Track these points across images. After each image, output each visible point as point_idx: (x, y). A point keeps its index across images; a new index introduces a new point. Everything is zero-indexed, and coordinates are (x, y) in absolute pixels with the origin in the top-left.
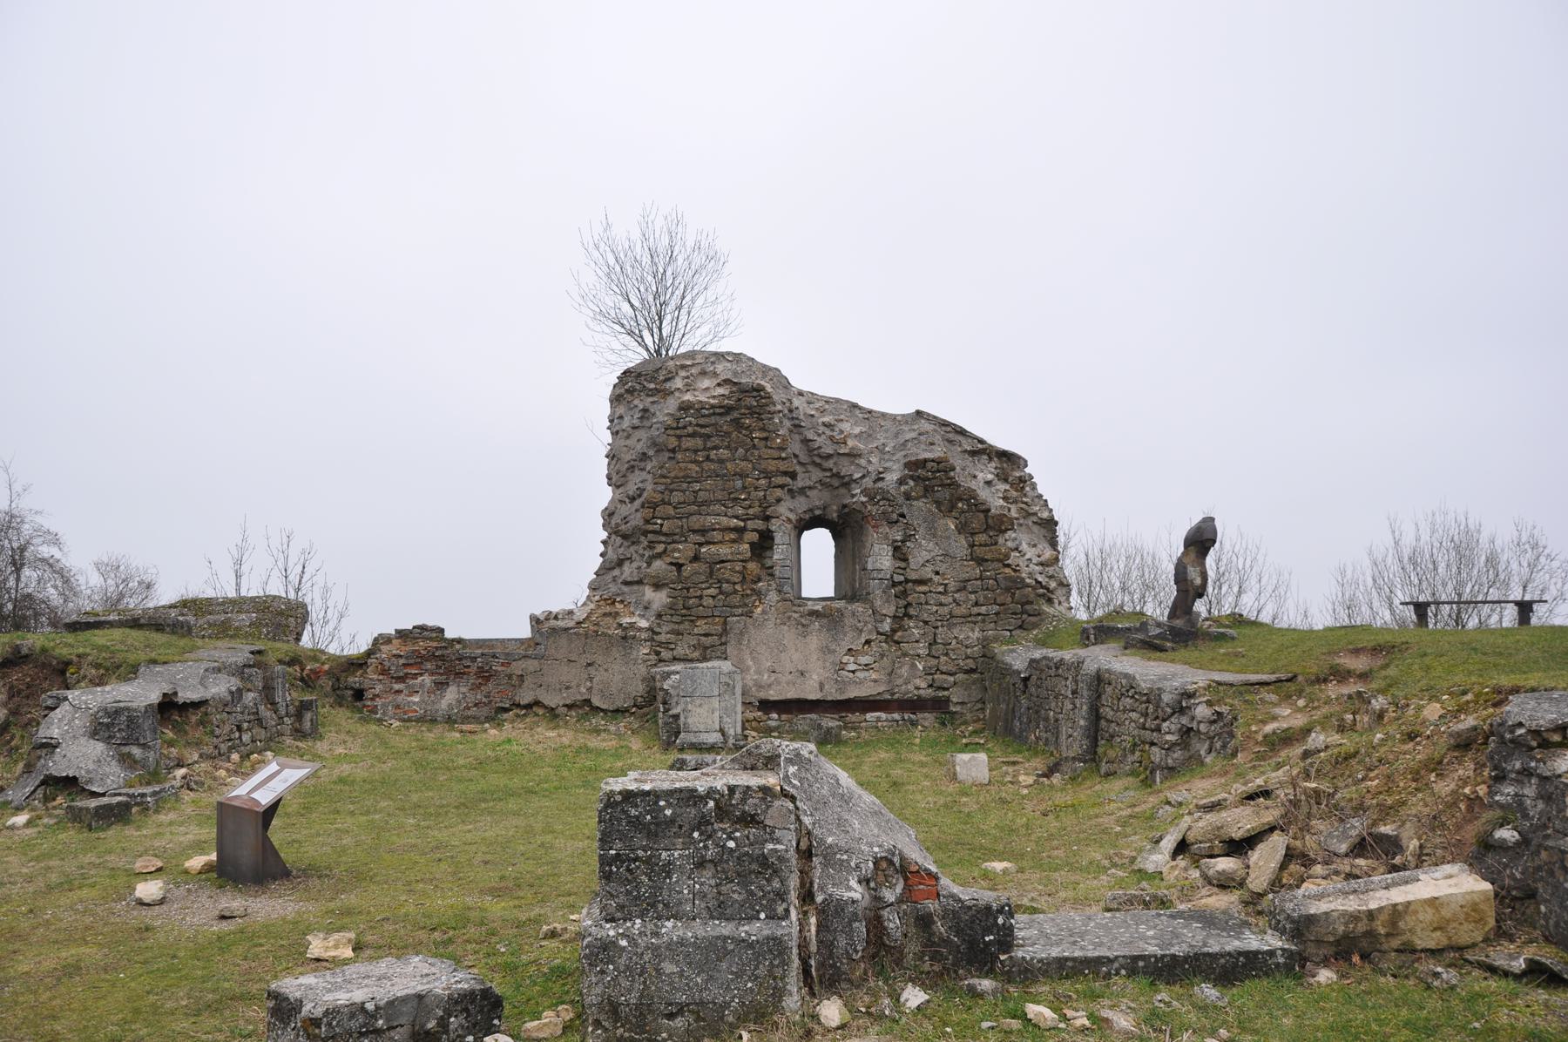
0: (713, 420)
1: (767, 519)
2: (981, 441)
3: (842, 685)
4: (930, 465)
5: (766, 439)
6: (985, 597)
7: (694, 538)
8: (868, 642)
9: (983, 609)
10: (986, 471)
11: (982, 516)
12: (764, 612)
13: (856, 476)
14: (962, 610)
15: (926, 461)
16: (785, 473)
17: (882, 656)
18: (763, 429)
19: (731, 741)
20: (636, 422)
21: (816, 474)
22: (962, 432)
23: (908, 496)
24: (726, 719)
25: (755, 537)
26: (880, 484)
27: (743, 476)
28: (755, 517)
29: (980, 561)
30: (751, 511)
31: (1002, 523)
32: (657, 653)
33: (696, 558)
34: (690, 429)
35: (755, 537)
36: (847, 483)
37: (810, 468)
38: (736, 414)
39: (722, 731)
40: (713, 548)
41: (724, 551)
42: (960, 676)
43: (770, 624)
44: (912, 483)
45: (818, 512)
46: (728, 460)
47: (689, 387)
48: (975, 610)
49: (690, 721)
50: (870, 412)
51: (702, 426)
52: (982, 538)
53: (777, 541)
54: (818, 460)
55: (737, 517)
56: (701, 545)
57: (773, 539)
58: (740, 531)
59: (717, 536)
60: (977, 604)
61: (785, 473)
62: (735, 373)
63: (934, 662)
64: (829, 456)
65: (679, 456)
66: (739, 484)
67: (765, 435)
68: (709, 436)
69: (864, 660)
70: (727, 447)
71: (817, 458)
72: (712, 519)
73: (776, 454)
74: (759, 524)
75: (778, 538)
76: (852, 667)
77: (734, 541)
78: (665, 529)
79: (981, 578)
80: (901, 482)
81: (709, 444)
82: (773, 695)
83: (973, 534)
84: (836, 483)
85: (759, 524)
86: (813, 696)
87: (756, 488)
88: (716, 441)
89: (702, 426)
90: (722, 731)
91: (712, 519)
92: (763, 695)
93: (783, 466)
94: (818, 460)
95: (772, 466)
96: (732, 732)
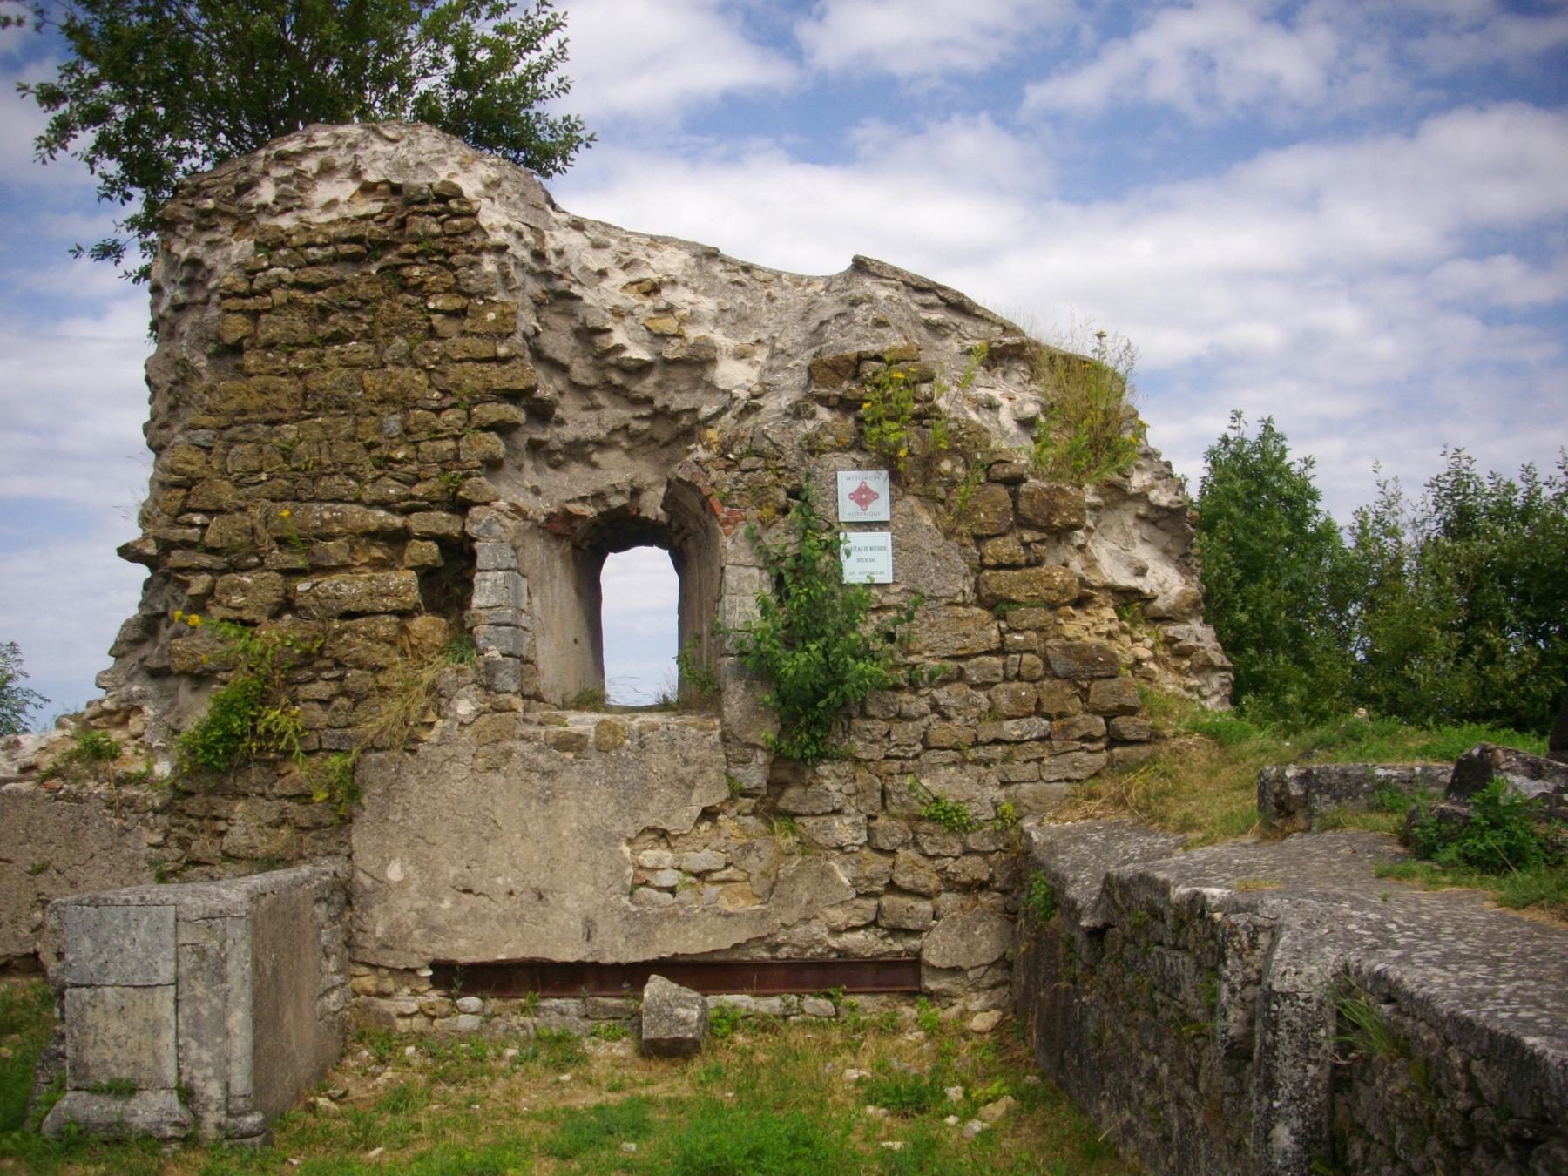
0: (335, 272)
1: (460, 507)
2: (1007, 328)
3: (646, 924)
4: (869, 368)
5: (460, 314)
6: (1014, 697)
7: (278, 557)
8: (708, 814)
9: (1011, 729)
10: (1013, 398)
11: (1002, 492)
12: (444, 740)
13: (706, 411)
14: (957, 730)
15: (861, 358)
16: (511, 396)
17: (747, 849)
18: (455, 290)
19: (212, 1118)
20: (181, 295)
21: (615, 413)
22: (960, 306)
23: (812, 447)
24: (194, 1051)
25: (429, 552)
26: (750, 422)
27: (404, 402)
28: (431, 505)
29: (996, 605)
30: (419, 490)
31: (1054, 509)
32: (184, 843)
33: (287, 605)
34: (279, 295)
35: (429, 552)
36: (687, 430)
37: (600, 398)
38: (391, 257)
39: (187, 1094)
40: (327, 583)
41: (350, 588)
42: (949, 900)
43: (460, 771)
44: (824, 414)
45: (617, 501)
46: (367, 366)
47: (286, 203)
48: (988, 731)
49: (90, 1056)
50: (747, 269)
51: (312, 288)
52: (1006, 547)
53: (482, 561)
54: (617, 378)
55: (385, 504)
56: (292, 573)
57: (472, 556)
58: (399, 538)
59: (335, 550)
60: (994, 713)
61: (511, 396)
62: (402, 167)
63: (878, 865)
64: (642, 369)
65: (251, 361)
66: (393, 423)
67: (457, 303)
68: (324, 312)
69: (701, 859)
70: (367, 336)
71: (617, 377)
72: (322, 513)
73: (483, 348)
74: (440, 521)
75: (485, 552)
76: (668, 878)
77: (380, 565)
78: (211, 537)
79: (1001, 651)
80: (798, 412)
81: (324, 330)
82: (466, 950)
83: (979, 539)
84: (664, 433)
85: (440, 521)
86: (569, 952)
87: (436, 435)
88: (340, 321)
89: (312, 288)
90: (187, 1094)
91: (322, 513)
92: (441, 949)
93: (500, 377)
94: (617, 378)
95: (471, 377)
96: (214, 1090)
